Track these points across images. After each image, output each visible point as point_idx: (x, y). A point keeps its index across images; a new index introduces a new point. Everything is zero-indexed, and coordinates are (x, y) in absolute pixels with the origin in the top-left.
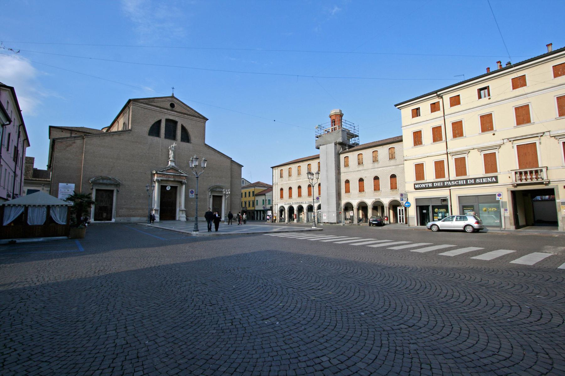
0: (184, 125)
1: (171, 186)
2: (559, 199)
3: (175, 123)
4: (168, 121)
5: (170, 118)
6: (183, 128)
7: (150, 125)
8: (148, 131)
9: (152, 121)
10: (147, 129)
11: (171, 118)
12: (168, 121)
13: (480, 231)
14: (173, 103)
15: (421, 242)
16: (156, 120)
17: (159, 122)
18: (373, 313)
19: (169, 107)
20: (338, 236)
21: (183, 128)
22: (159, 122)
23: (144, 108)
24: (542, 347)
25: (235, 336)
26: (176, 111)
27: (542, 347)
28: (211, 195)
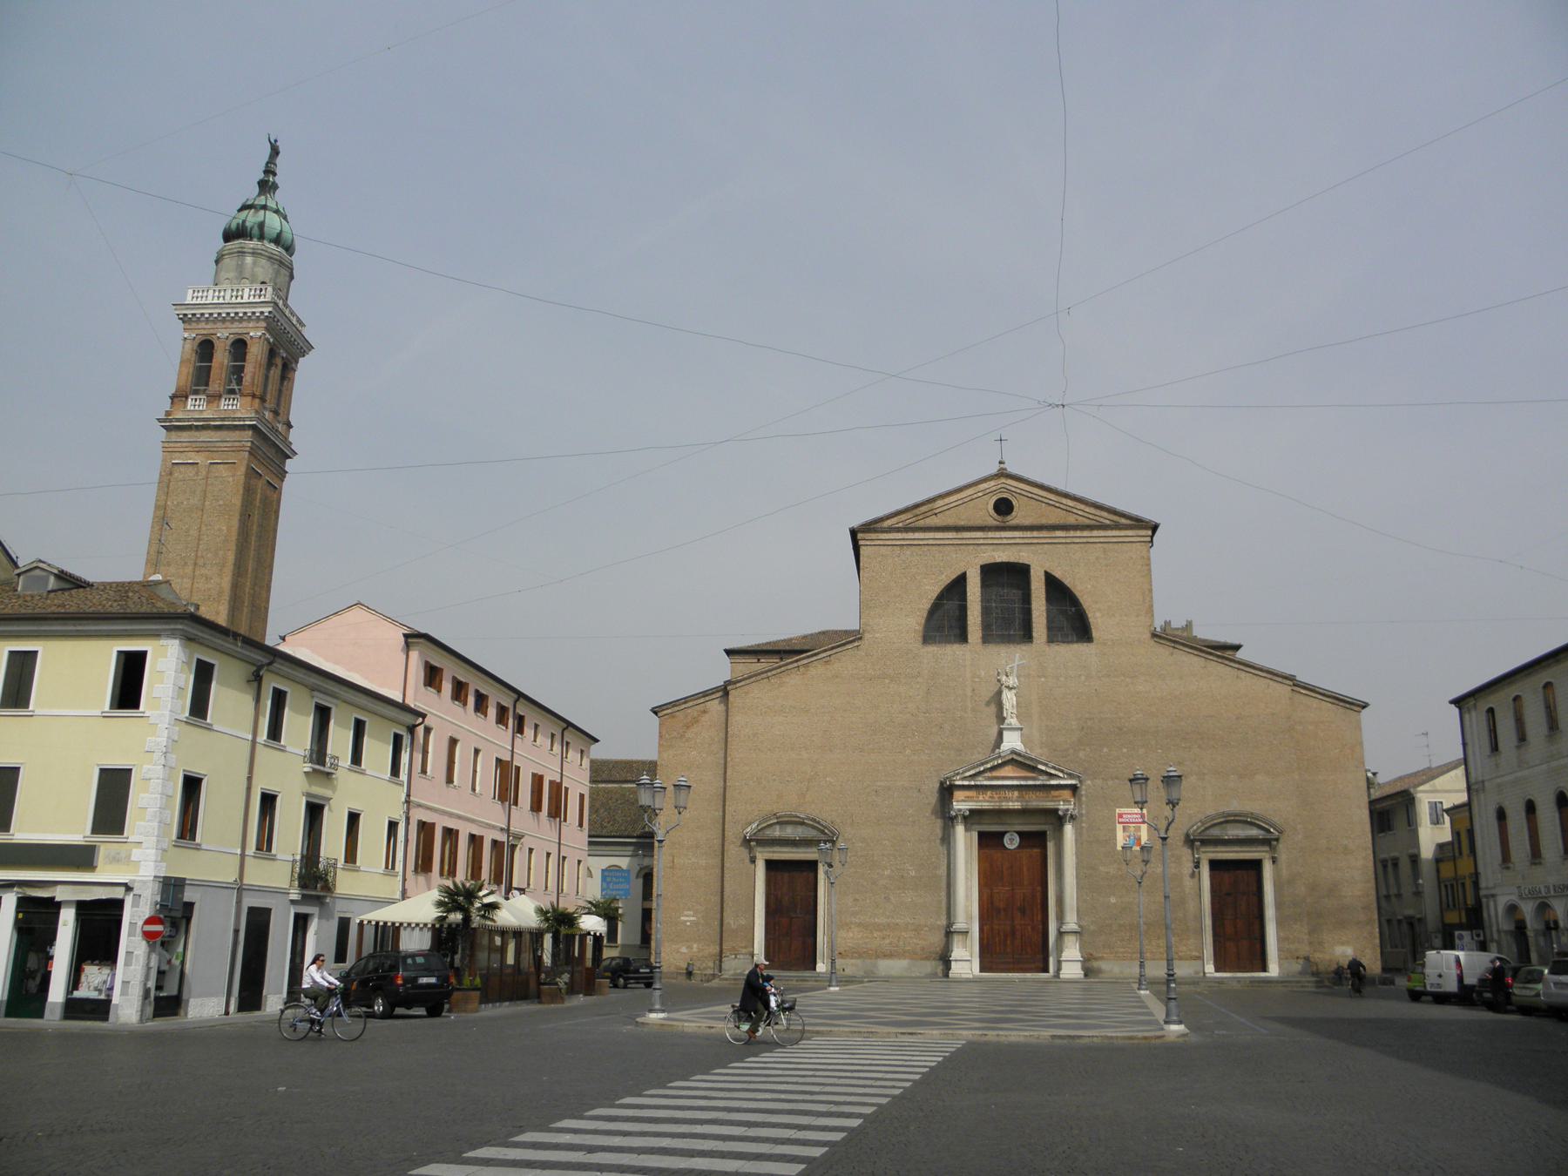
0: (1057, 574)
1: (1020, 834)
9: (932, 589)
10: (913, 619)
11: (1001, 556)
12: (991, 572)
19: (990, 517)
21: (1054, 586)
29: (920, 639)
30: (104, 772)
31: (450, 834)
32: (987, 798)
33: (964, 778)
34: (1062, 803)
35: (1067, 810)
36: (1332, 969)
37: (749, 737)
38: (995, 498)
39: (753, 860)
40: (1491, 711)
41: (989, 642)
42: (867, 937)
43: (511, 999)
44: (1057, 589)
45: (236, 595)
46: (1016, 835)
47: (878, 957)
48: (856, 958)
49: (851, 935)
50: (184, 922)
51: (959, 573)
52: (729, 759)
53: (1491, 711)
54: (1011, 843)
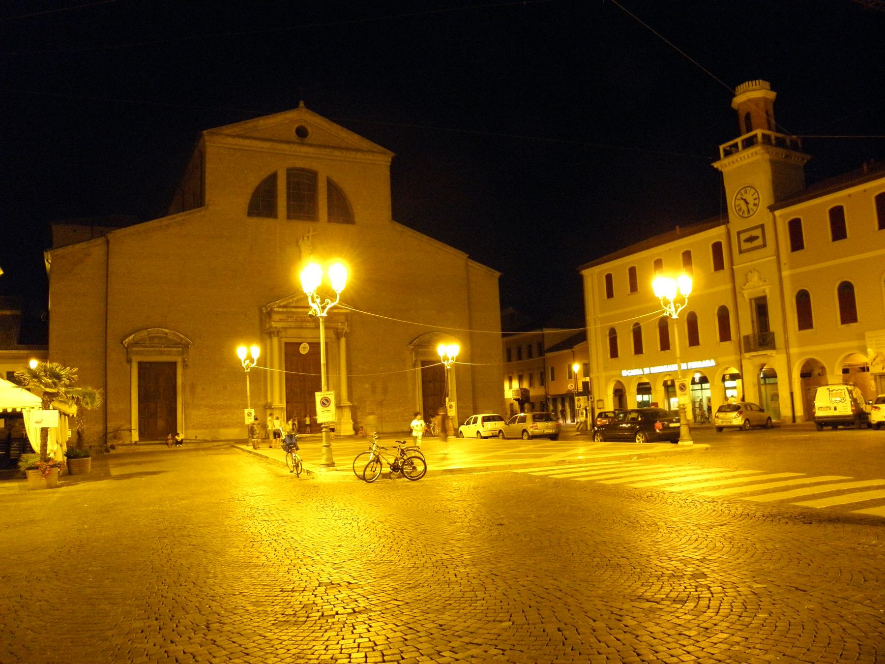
0: (335, 179)
1: (309, 344)
2: (777, 354)
3: (313, 176)
4: (292, 173)
5: (154, 221)
6: (331, 186)
7: (250, 191)
8: (246, 206)
9: (254, 180)
10: (243, 201)
11: (300, 164)
12: (292, 173)
13: (738, 429)
14: (303, 124)
15: (823, 475)
16: (264, 174)
17: (273, 178)
18: (705, 650)
19: (293, 136)
20: (859, 477)
21: (331, 186)
22: (273, 178)
23: (234, 149)
24: (700, 647)
25: (343, 651)
26: (311, 145)
27: (700, 647)
28: (416, 361)
29: (246, 214)
30: (855, 320)
31: (530, 356)
32: (293, 320)
33: (280, 307)
34: (340, 324)
35: (344, 329)
36: (424, 424)
37: (124, 274)
38: (296, 126)
39: (129, 361)
40: (609, 278)
41: (298, 218)
42: (212, 414)
43: (788, 472)
44: (333, 189)
45: (202, 158)
46: (307, 345)
47: (219, 427)
48: (204, 428)
49: (201, 413)
50: (579, 429)
51: (269, 173)
52: (109, 290)
53: (609, 278)
54: (304, 351)
